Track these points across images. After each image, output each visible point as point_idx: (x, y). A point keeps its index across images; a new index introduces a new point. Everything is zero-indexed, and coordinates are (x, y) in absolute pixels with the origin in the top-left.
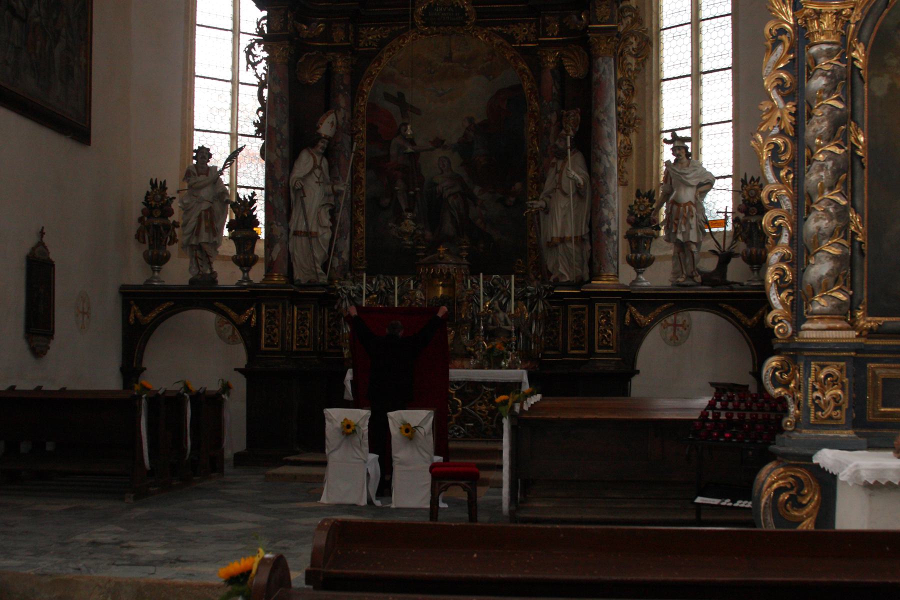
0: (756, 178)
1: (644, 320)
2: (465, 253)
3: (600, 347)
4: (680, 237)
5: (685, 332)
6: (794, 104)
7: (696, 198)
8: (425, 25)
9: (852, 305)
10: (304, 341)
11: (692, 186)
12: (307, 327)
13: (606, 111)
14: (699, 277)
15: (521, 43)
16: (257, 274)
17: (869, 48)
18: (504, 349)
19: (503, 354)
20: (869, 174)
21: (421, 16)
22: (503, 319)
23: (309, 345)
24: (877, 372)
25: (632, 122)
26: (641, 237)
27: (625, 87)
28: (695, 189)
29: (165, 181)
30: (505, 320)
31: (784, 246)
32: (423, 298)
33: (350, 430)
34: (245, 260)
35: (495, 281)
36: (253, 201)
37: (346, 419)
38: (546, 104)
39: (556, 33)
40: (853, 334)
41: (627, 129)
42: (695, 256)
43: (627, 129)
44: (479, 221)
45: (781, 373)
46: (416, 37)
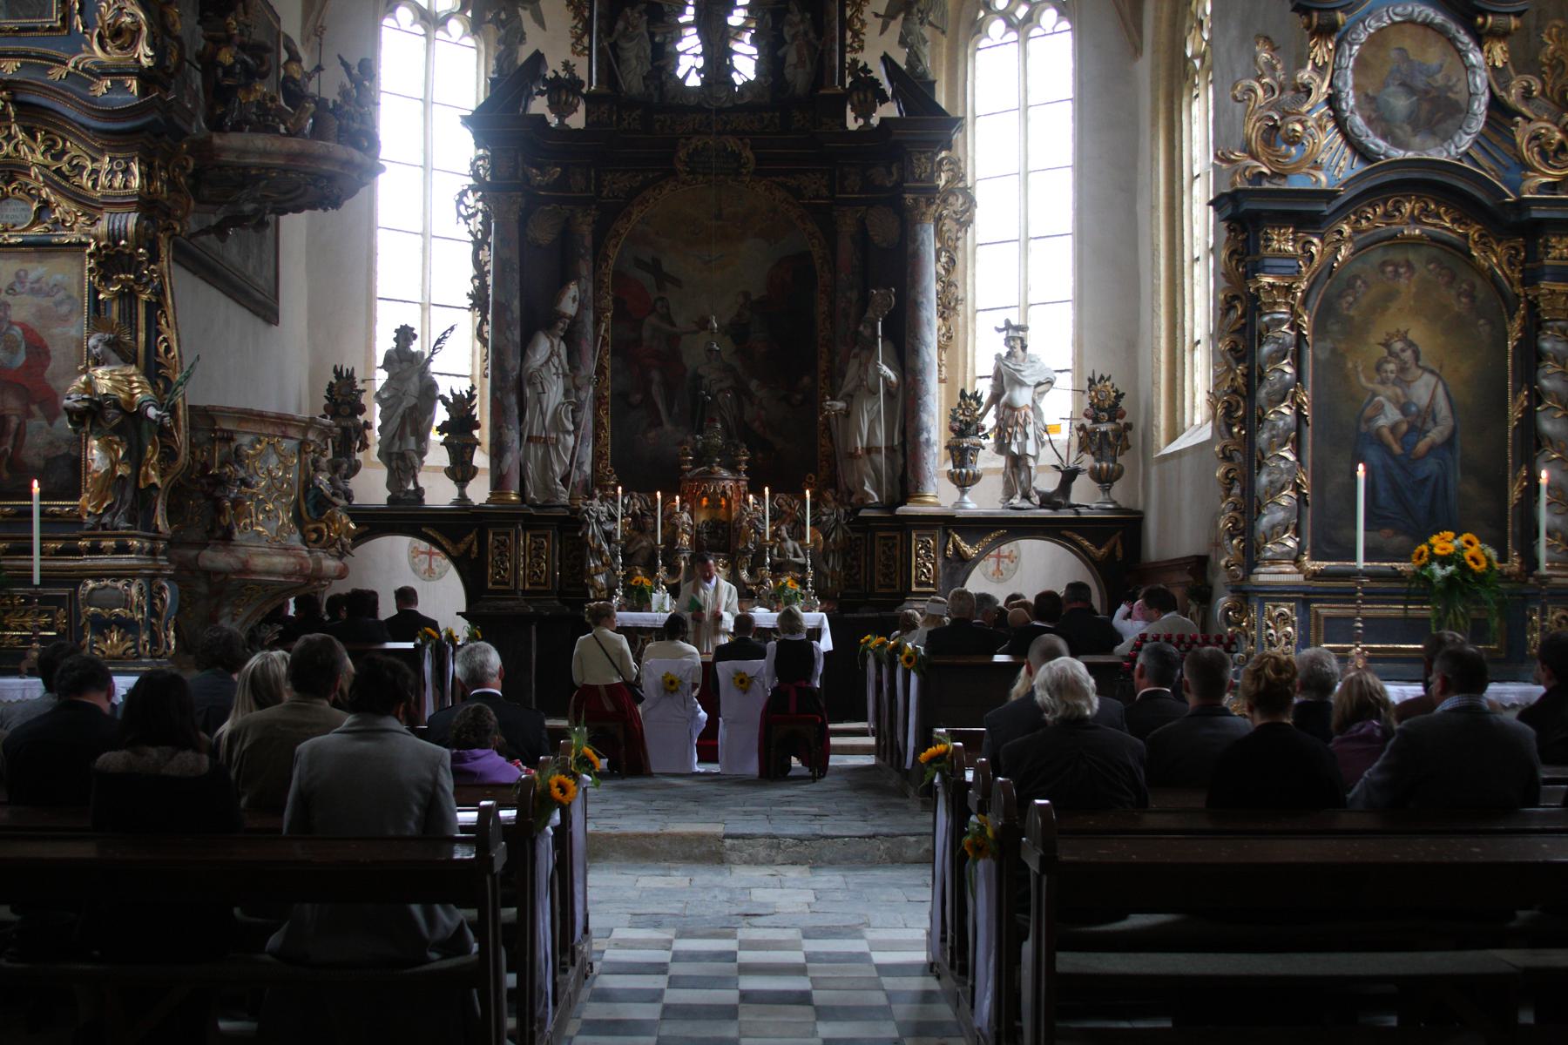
0: (1106, 377)
1: (970, 551)
3: (919, 584)
4: (1014, 449)
5: (1012, 566)
6: (1246, 365)
7: (1034, 401)
8: (689, 173)
9: (1301, 550)
10: (540, 578)
11: (1029, 386)
13: (925, 291)
14: (1037, 497)
15: (810, 199)
16: (479, 491)
17: (1313, 316)
18: (798, 588)
19: (796, 594)
20: (1312, 430)
23: (546, 581)
24: (1320, 611)
25: (952, 304)
26: (967, 448)
27: (943, 260)
28: (1032, 389)
29: (353, 369)
31: (1235, 495)
32: (691, 522)
33: (673, 688)
34: (461, 471)
35: (781, 501)
36: (472, 396)
37: (668, 674)
39: (857, 189)
40: (1301, 577)
41: (947, 312)
42: (1033, 471)
43: (947, 312)
44: (757, 424)
45: (1234, 613)
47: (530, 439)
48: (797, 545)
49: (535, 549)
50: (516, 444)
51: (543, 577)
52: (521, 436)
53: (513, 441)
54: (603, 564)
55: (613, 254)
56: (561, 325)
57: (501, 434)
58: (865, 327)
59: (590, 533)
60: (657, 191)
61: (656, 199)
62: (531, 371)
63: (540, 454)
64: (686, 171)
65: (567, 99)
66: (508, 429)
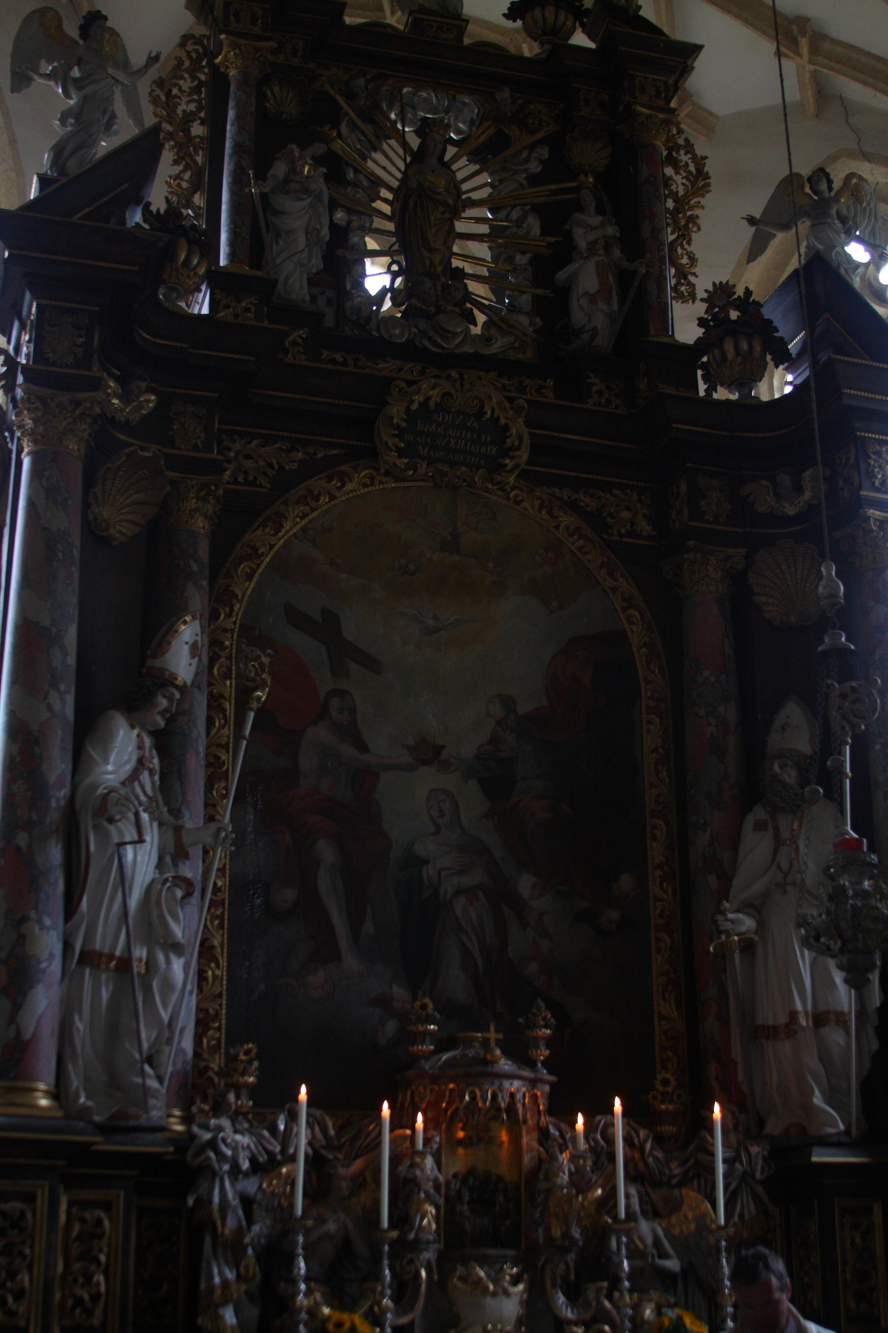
2: (543, 1053)
8: (401, 453)
10: (90, 1313)
12: (99, 1263)
21: (398, 427)
22: (649, 1240)
30: (657, 1243)
38: (712, 678)
44: (533, 967)
46: (372, 479)
47: (88, 958)
48: (660, 1231)
49: (79, 1237)
50: (56, 967)
51: (99, 1311)
52: (67, 946)
53: (51, 956)
54: (239, 1277)
55: (245, 589)
56: (164, 703)
57: (22, 939)
58: (782, 767)
59: (216, 1199)
60: (336, 483)
61: (332, 497)
62: (101, 791)
63: (105, 995)
64: (398, 449)
65: (188, 260)
66: (42, 927)
